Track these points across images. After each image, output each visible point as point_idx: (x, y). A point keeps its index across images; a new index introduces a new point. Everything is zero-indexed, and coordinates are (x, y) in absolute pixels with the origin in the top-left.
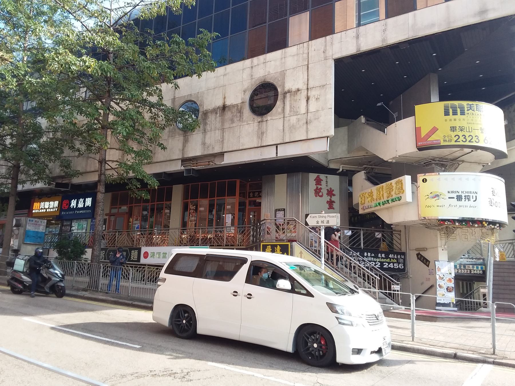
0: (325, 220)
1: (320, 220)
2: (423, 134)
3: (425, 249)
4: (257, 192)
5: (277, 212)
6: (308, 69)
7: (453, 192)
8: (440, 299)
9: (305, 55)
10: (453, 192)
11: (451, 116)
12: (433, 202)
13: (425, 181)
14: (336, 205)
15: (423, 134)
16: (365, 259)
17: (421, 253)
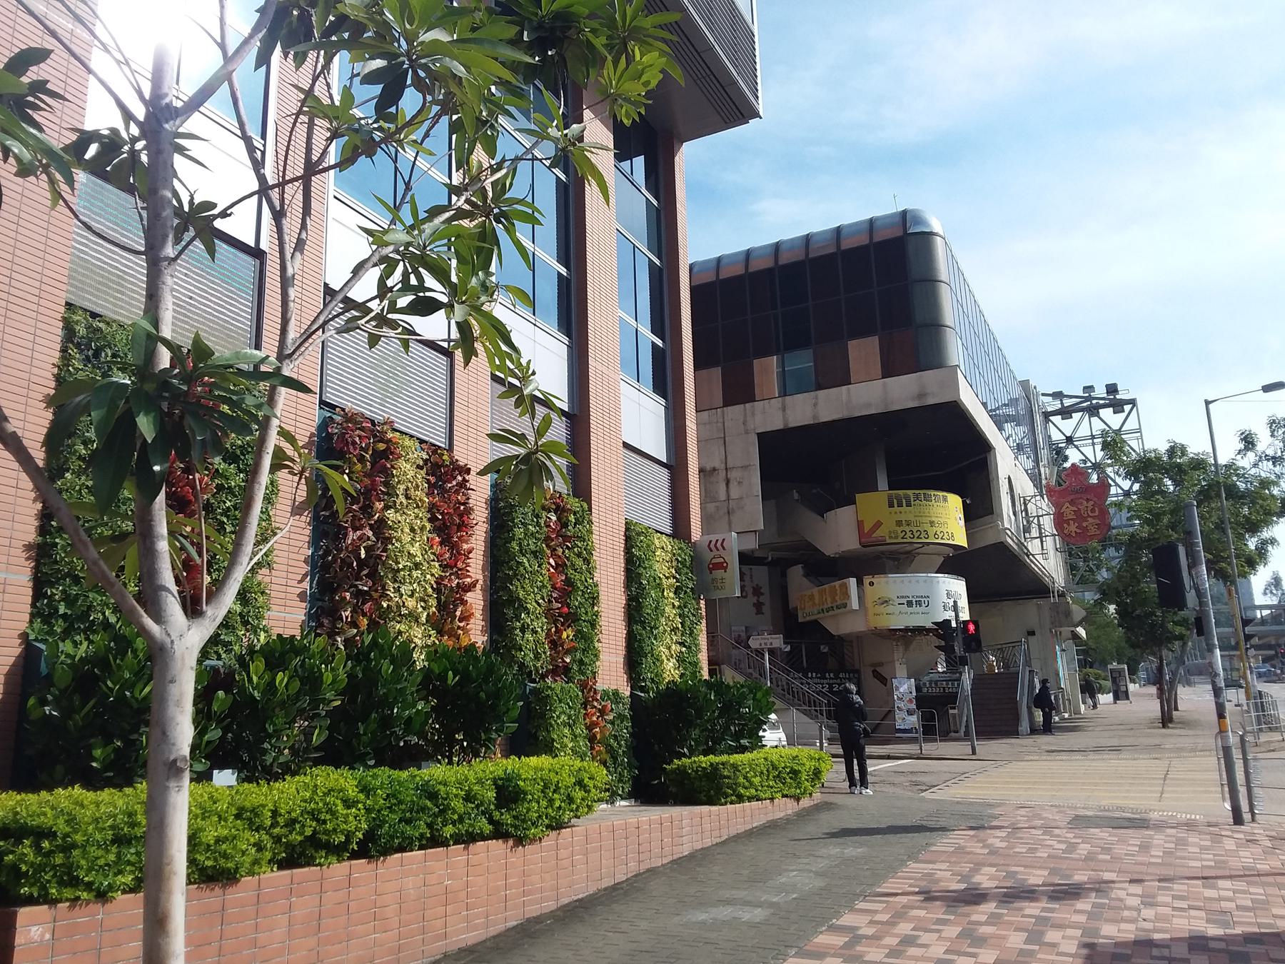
0: (769, 642)
1: (763, 642)
2: (867, 529)
3: (881, 664)
6: (725, 443)
7: (902, 597)
8: (900, 725)
9: (720, 425)
10: (902, 597)
11: (896, 508)
12: (882, 609)
13: (871, 584)
14: (766, 609)
15: (867, 529)
16: (809, 681)
17: (877, 669)
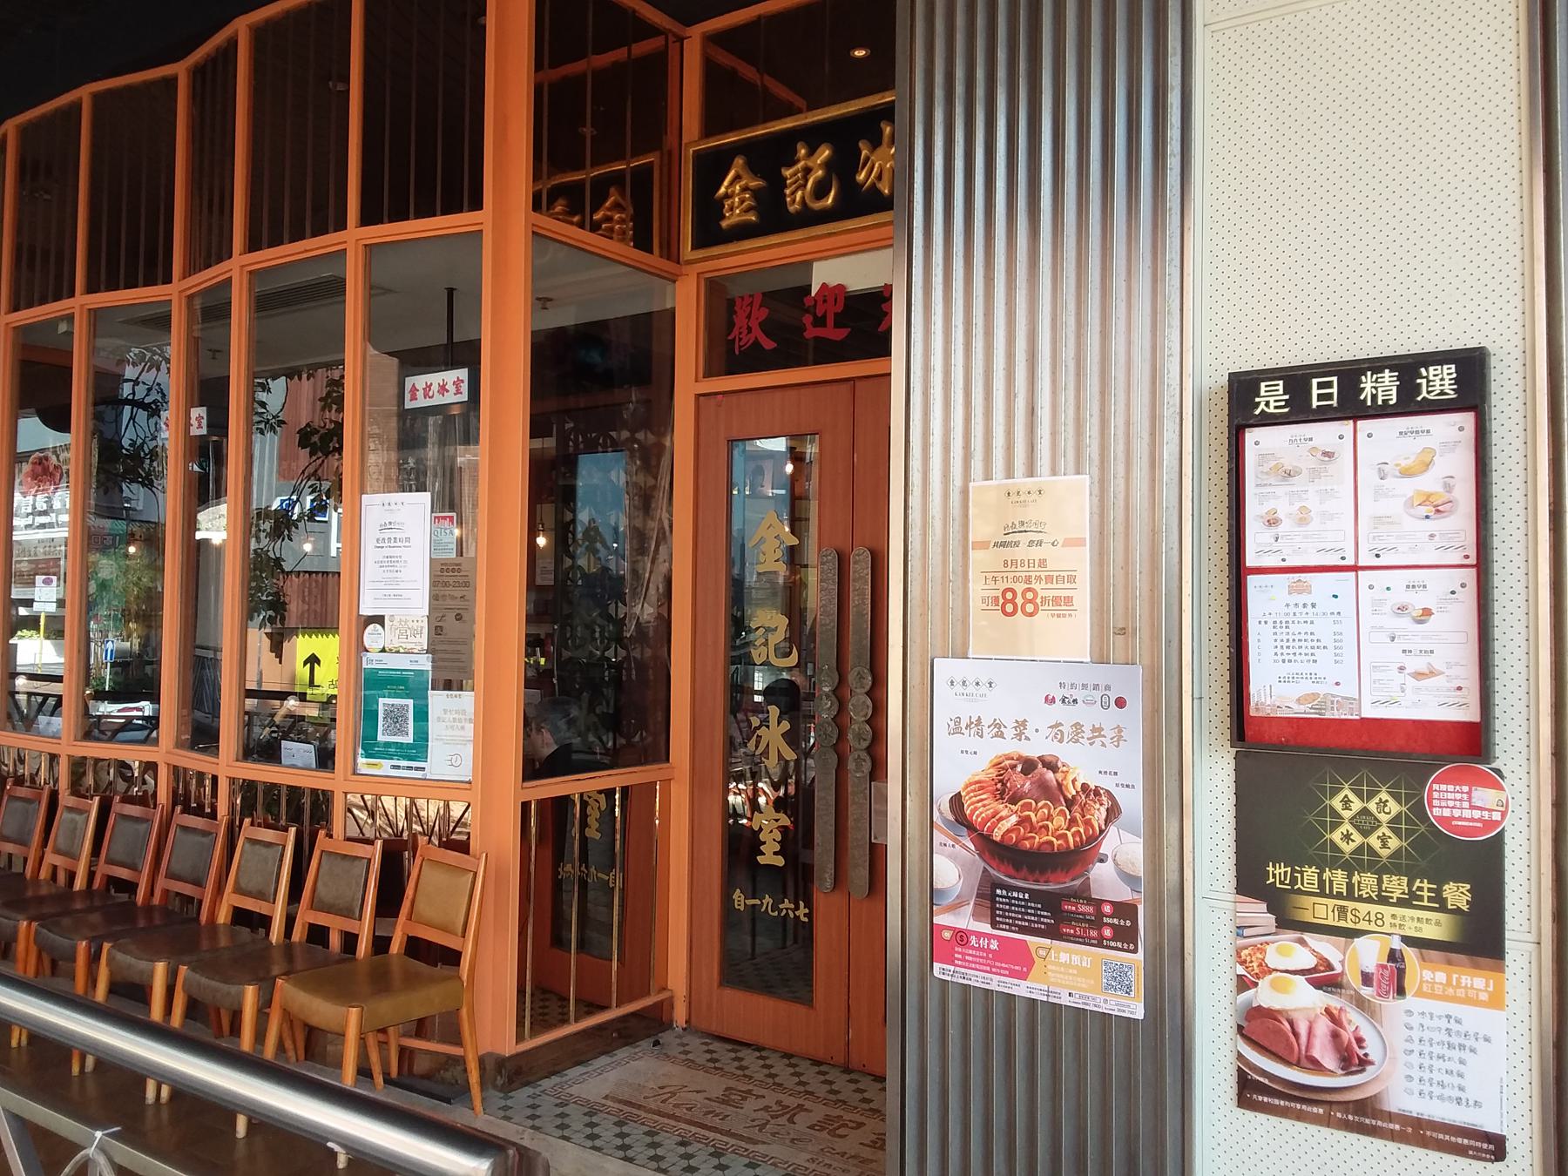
4: (813, 136)
5: (1258, 441)
